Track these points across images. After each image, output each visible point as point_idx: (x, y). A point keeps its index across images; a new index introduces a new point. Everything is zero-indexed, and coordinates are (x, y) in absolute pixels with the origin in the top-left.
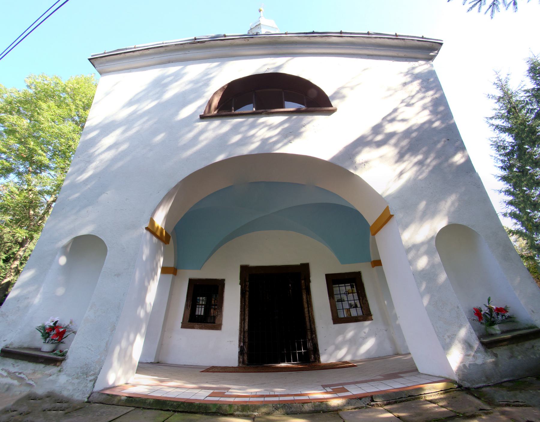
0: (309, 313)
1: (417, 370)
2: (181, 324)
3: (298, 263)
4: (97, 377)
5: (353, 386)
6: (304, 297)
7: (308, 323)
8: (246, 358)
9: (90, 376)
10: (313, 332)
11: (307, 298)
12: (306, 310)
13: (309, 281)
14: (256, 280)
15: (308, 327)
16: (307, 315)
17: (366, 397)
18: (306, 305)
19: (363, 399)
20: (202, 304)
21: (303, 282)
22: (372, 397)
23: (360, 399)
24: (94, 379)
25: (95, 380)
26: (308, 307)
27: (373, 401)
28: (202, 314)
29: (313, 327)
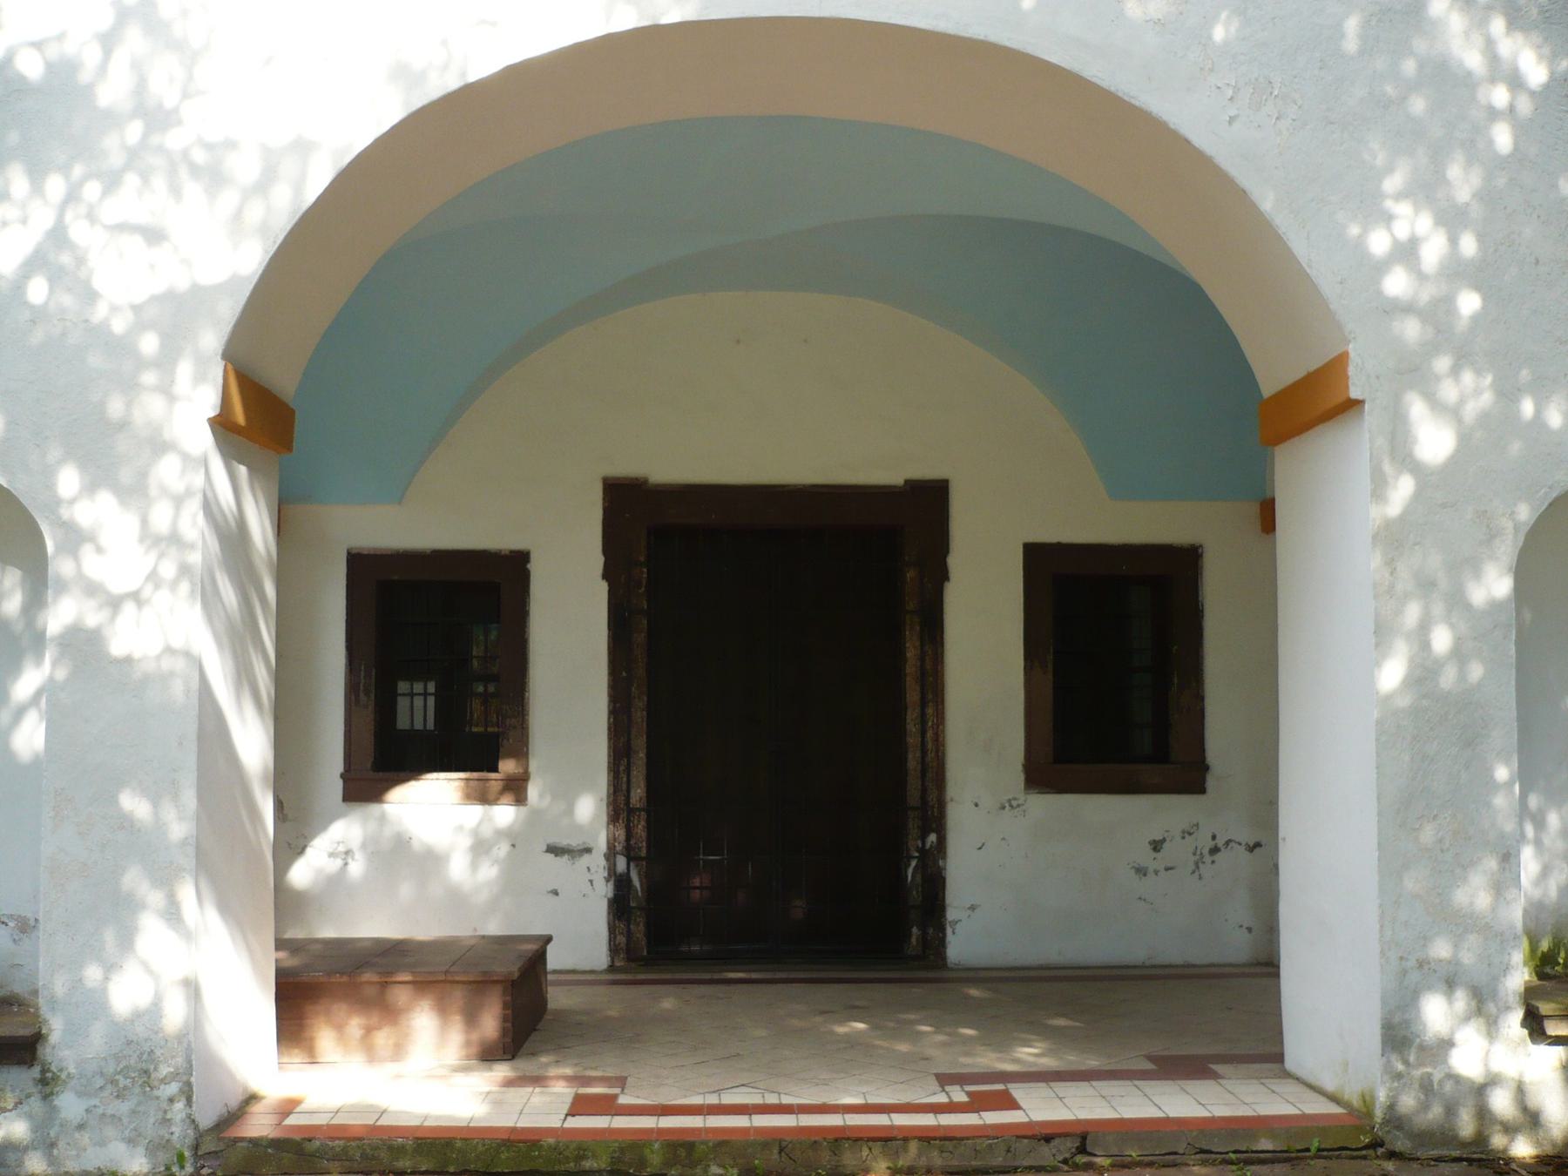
0: (923, 733)
1: (1279, 1058)
2: (340, 783)
3: (891, 475)
4: (189, 1084)
5: (1041, 1089)
6: (911, 653)
7: (913, 784)
8: (639, 930)
9: (163, 1081)
10: (934, 818)
11: (922, 659)
12: (912, 715)
13: (943, 575)
14: (669, 543)
15: (913, 797)
16: (912, 740)
17: (1066, 1135)
18: (912, 696)
19: (1056, 1142)
20: (419, 666)
21: (910, 574)
22: (1084, 1138)
23: (1048, 1139)
24: (181, 1091)
25: (188, 1093)
26: (923, 703)
27: (1082, 1150)
28: (431, 725)
29: (932, 797)
